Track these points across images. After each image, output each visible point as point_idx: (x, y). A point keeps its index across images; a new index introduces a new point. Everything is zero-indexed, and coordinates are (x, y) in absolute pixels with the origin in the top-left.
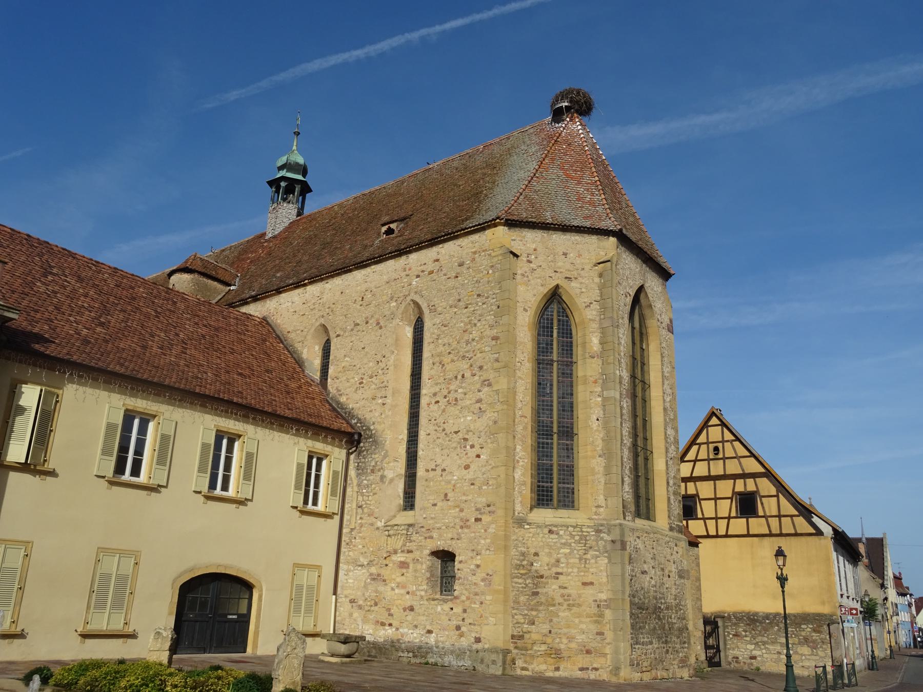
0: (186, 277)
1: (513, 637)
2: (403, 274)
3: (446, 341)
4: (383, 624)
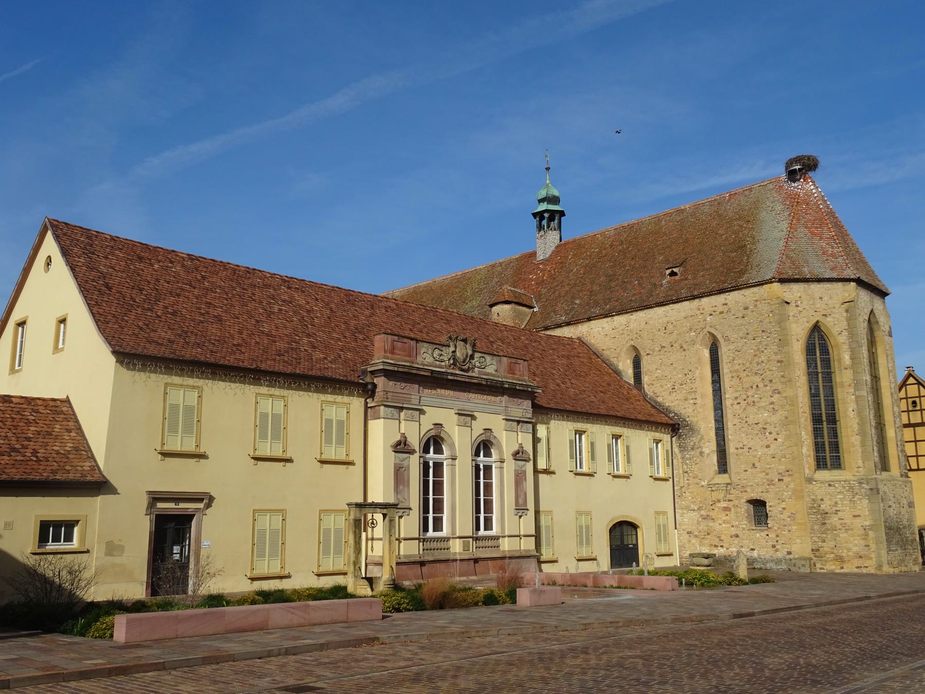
0: (507, 307)
1: (813, 550)
3: (740, 361)
4: (716, 546)
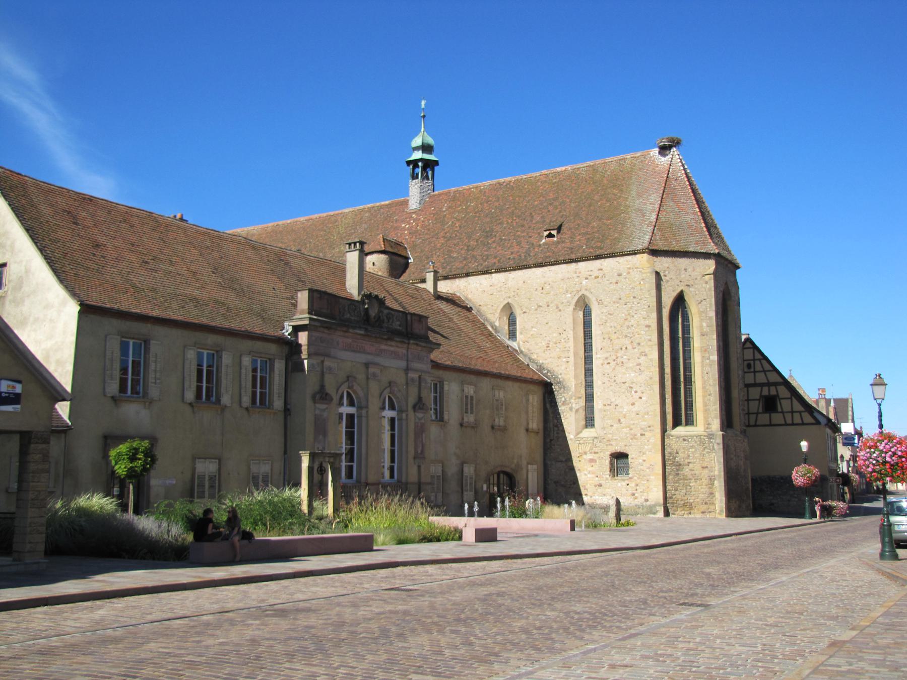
2: (575, 275)
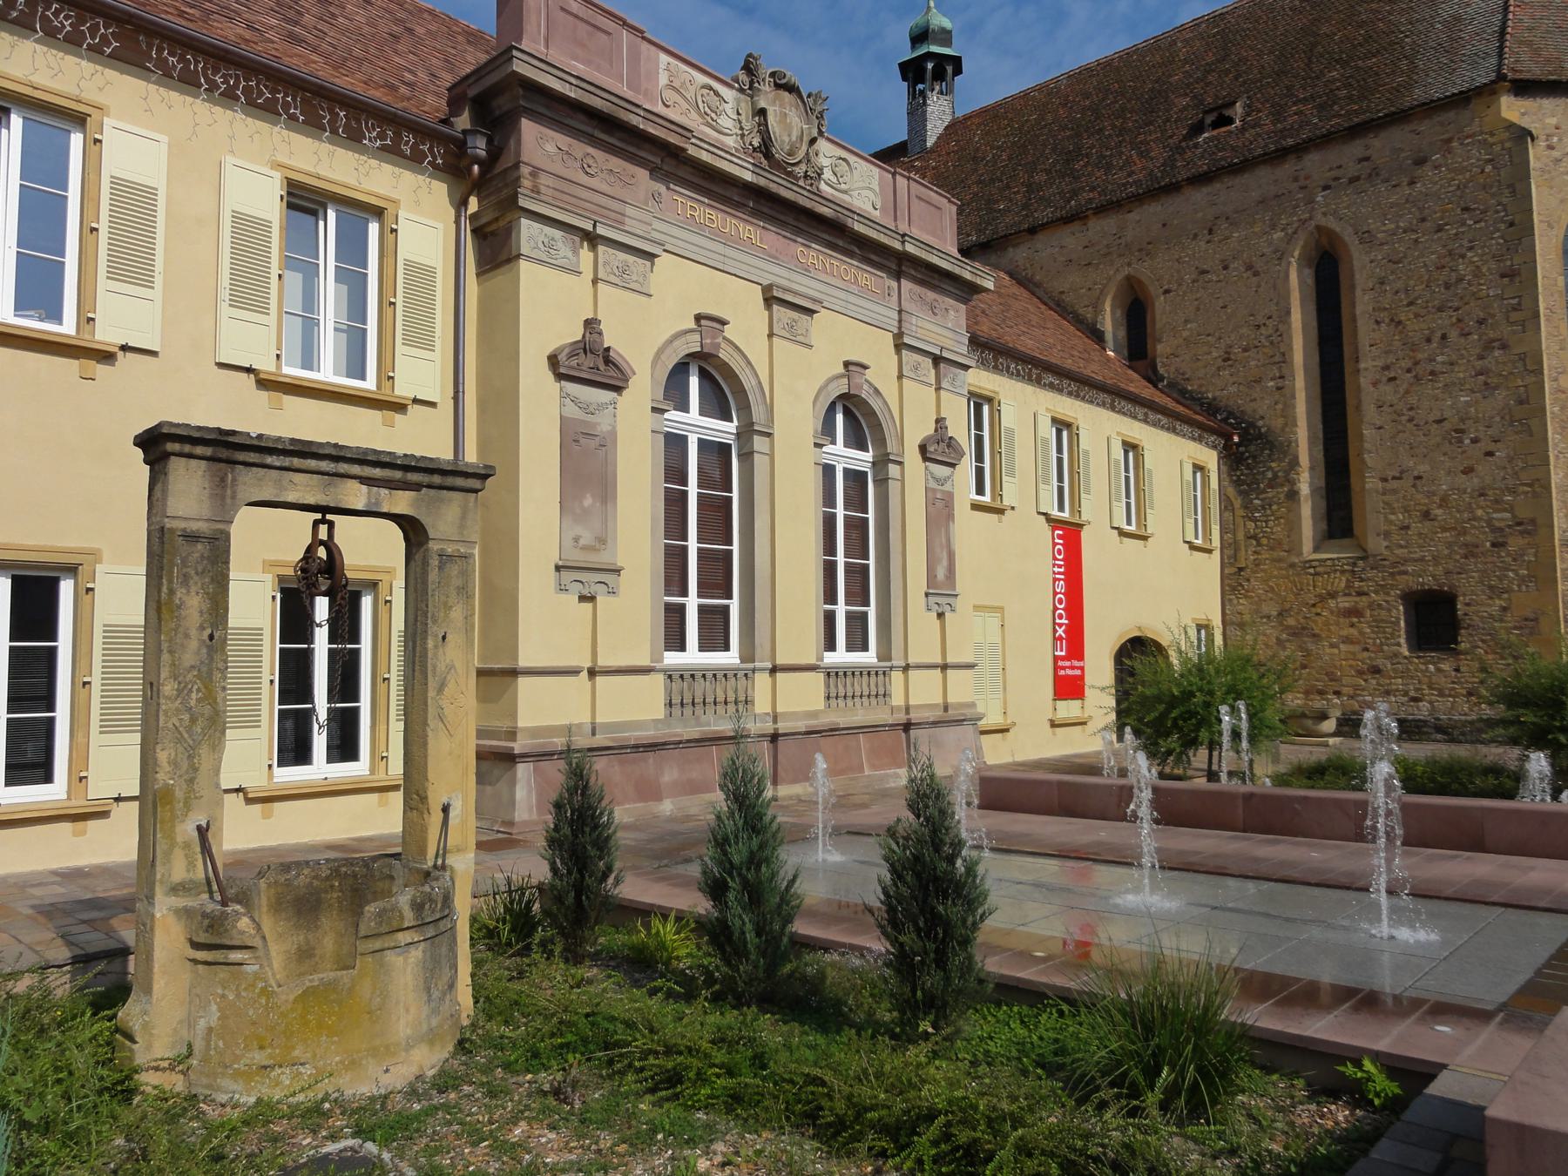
3: (1399, 285)
